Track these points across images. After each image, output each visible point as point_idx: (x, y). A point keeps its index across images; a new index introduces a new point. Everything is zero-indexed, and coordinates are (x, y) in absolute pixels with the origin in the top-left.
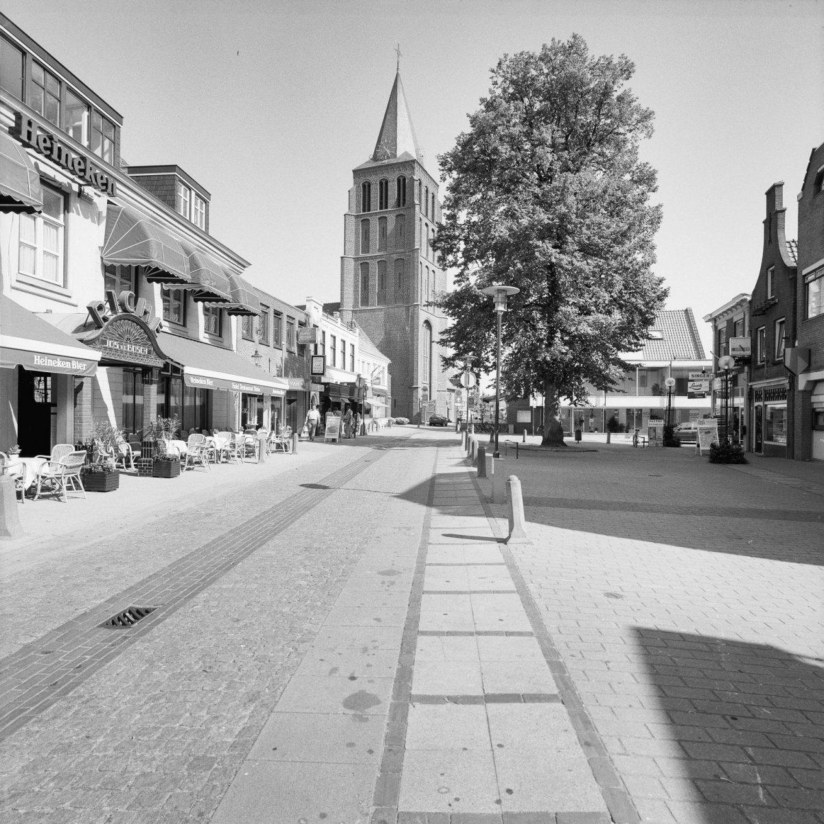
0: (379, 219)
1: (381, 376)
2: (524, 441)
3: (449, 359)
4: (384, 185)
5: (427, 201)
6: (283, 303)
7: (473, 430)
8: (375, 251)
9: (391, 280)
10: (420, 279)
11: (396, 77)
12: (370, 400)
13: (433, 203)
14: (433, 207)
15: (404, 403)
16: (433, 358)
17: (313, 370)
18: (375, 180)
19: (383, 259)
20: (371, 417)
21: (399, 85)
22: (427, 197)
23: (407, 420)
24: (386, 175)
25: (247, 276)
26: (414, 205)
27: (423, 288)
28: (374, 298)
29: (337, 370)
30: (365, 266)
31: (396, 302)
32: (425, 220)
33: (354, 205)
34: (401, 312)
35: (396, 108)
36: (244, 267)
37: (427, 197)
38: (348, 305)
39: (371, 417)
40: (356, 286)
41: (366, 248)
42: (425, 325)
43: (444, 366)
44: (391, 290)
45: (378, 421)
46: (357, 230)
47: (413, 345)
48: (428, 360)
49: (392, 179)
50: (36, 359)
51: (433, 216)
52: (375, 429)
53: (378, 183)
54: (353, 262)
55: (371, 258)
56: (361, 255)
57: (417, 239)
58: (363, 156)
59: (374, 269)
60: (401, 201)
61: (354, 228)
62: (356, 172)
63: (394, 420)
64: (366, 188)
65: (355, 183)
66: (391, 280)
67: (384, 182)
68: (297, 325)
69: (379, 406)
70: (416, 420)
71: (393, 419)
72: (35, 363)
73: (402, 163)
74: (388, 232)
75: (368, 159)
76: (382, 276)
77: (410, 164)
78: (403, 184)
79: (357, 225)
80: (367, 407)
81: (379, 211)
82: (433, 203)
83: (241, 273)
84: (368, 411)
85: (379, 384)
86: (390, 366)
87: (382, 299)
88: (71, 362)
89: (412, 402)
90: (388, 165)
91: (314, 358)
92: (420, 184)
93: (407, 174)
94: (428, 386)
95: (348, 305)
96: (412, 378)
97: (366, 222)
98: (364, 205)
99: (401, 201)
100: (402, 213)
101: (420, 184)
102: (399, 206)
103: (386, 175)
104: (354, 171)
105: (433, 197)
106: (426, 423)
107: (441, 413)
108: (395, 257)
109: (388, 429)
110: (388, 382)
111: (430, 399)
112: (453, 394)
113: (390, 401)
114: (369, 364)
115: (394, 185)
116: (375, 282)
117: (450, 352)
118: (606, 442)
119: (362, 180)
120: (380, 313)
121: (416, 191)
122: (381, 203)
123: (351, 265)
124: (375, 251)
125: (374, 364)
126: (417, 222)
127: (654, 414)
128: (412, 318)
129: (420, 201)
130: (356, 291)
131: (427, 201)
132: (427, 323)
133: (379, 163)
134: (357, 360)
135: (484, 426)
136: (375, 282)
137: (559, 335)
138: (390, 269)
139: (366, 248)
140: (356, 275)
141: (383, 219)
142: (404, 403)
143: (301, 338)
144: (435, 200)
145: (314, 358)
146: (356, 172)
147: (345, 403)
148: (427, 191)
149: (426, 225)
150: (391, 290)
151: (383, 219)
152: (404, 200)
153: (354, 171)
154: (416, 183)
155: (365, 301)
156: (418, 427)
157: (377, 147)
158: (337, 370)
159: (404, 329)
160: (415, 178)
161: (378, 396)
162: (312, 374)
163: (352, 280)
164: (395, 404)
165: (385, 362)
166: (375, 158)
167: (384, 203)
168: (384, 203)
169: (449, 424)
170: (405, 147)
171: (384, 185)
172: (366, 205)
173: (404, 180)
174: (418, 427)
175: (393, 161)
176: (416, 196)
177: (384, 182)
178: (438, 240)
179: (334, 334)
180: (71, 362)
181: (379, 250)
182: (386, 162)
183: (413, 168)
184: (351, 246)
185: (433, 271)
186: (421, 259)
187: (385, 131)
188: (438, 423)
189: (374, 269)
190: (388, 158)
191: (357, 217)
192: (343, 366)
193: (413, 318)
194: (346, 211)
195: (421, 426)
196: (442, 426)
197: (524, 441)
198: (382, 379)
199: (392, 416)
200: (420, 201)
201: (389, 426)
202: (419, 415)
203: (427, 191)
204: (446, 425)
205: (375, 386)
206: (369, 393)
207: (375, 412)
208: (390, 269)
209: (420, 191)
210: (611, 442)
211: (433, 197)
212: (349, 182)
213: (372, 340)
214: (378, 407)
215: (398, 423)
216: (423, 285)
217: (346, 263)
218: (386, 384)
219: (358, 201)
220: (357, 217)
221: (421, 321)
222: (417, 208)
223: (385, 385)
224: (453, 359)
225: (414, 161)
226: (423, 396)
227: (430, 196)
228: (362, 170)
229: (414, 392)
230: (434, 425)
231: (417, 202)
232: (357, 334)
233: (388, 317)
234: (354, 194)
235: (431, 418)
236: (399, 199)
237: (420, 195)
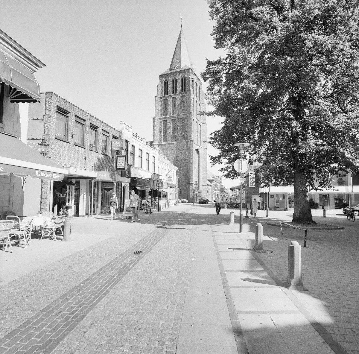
0: (172, 98)
1: (172, 176)
2: (267, 216)
3: (216, 157)
4: (175, 82)
5: (196, 90)
6: (99, 120)
7: (226, 206)
8: (170, 114)
9: (178, 129)
10: (193, 128)
11: (181, 32)
12: (165, 189)
13: (200, 91)
14: (199, 93)
15: (185, 192)
16: (200, 169)
17: (118, 165)
18: (170, 79)
19: (175, 118)
20: (167, 199)
21: (182, 34)
22: (196, 88)
23: (187, 201)
24: (176, 77)
25: (39, 75)
26: (190, 90)
27: (195, 133)
28: (170, 137)
29: (143, 170)
30: (165, 122)
31: (181, 140)
32: (195, 99)
33: (160, 92)
34: (183, 144)
35: (181, 45)
36: (38, 66)
37: (196, 88)
38: (156, 142)
39: (167, 199)
40: (161, 132)
41: (166, 113)
42: (196, 151)
43: (212, 162)
44: (178, 133)
45: (170, 201)
46: (161, 104)
47: (190, 161)
48: (198, 169)
49: (179, 78)
50: (36, 173)
51: (199, 98)
52: (167, 207)
53: (172, 81)
54: (159, 120)
55: (168, 118)
56: (163, 116)
57: (191, 107)
58: (165, 69)
59: (170, 124)
60: (183, 89)
61: (159, 103)
62: (161, 76)
63: (180, 200)
64: (166, 84)
65: (160, 81)
66: (178, 129)
67: (175, 80)
68: (111, 137)
69: (172, 194)
70: (192, 201)
71: (179, 200)
72: (36, 175)
73: (183, 70)
74: (177, 105)
75: (167, 70)
76: (175, 127)
77: (188, 70)
78: (184, 81)
79: (161, 102)
80: (164, 193)
81: (172, 94)
82: (200, 91)
83: (35, 71)
84: (165, 196)
85: (171, 181)
86: (177, 171)
87: (174, 138)
88: (52, 174)
89: (190, 191)
90: (177, 72)
91: (118, 157)
92: (193, 81)
93: (186, 75)
94: (198, 183)
95: (156, 142)
96: (190, 179)
97: (166, 100)
98: (165, 92)
99: (183, 89)
100: (184, 95)
101: (193, 81)
102: (182, 91)
103: (176, 77)
104: (160, 76)
105: (199, 88)
106: (197, 202)
107: (204, 197)
108: (180, 117)
109: (176, 206)
110: (177, 180)
111: (199, 190)
112: (210, 187)
113: (178, 190)
114: (162, 168)
115: (180, 84)
116: (170, 130)
117: (216, 152)
118: (322, 215)
119: (164, 80)
120: (173, 145)
121: (191, 83)
122: (173, 91)
123: (158, 121)
124: (170, 114)
125: (169, 170)
126: (191, 99)
127: (102, 191)
128: (189, 148)
129: (193, 88)
130: (161, 135)
131: (196, 90)
132: (197, 150)
133: (172, 71)
134: (154, 165)
135: (232, 205)
136: (170, 130)
137: (310, 131)
138: (178, 123)
139: (166, 113)
140: (161, 127)
141: (174, 98)
142: (185, 192)
143: (113, 146)
144: (201, 90)
145: (118, 157)
146: (161, 76)
147: (148, 192)
148: (196, 85)
149: (196, 101)
150: (178, 133)
151: (174, 98)
152: (185, 89)
153: (160, 76)
154: (191, 80)
155: (165, 139)
156: (193, 204)
157: (171, 64)
158: (143, 170)
159: (185, 153)
160: (190, 77)
161: (171, 187)
162: (117, 169)
163: (159, 129)
164: (180, 192)
165: (175, 169)
166: (170, 69)
167: (175, 91)
168: (175, 91)
169: (209, 202)
170: (185, 64)
171: (175, 82)
172: (166, 92)
173: (185, 79)
174: (193, 204)
175: (179, 70)
176: (191, 86)
177: (175, 80)
178: (208, 72)
179: (148, 152)
180: (52, 174)
181: (173, 114)
182: (176, 70)
183: (189, 73)
184: (158, 112)
185: (200, 125)
186: (194, 118)
187: (175, 56)
188: (204, 202)
189: (170, 124)
190: (177, 68)
191: (161, 98)
192: (147, 169)
193: (190, 147)
194: (156, 95)
195: (195, 204)
196: (206, 204)
197: (267, 216)
198: (173, 178)
199: (179, 199)
200: (193, 88)
201: (177, 204)
202: (193, 197)
203: (196, 85)
204: (208, 203)
205: (169, 182)
206: (165, 186)
207: (169, 196)
208: (178, 123)
209: (193, 84)
210: (326, 216)
211: (199, 88)
212: (157, 81)
213: (169, 159)
214: (171, 194)
215: (182, 202)
216: (195, 135)
217: (155, 120)
218: (175, 181)
219: (162, 90)
220: (161, 98)
221: (194, 149)
222: (191, 92)
223: (175, 181)
224: (220, 157)
225: (190, 69)
226: (196, 187)
227: (198, 88)
228: (165, 74)
229: (191, 185)
230: (201, 203)
231: (191, 89)
232: (157, 151)
233: (177, 148)
234: (160, 87)
235: (200, 199)
236: (182, 89)
237: (193, 86)
